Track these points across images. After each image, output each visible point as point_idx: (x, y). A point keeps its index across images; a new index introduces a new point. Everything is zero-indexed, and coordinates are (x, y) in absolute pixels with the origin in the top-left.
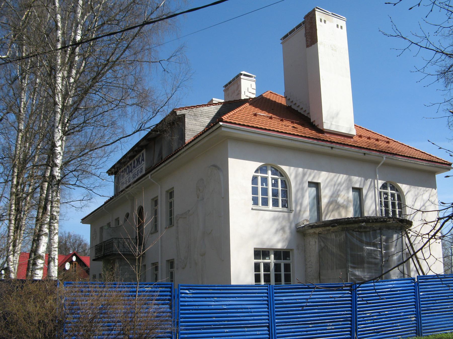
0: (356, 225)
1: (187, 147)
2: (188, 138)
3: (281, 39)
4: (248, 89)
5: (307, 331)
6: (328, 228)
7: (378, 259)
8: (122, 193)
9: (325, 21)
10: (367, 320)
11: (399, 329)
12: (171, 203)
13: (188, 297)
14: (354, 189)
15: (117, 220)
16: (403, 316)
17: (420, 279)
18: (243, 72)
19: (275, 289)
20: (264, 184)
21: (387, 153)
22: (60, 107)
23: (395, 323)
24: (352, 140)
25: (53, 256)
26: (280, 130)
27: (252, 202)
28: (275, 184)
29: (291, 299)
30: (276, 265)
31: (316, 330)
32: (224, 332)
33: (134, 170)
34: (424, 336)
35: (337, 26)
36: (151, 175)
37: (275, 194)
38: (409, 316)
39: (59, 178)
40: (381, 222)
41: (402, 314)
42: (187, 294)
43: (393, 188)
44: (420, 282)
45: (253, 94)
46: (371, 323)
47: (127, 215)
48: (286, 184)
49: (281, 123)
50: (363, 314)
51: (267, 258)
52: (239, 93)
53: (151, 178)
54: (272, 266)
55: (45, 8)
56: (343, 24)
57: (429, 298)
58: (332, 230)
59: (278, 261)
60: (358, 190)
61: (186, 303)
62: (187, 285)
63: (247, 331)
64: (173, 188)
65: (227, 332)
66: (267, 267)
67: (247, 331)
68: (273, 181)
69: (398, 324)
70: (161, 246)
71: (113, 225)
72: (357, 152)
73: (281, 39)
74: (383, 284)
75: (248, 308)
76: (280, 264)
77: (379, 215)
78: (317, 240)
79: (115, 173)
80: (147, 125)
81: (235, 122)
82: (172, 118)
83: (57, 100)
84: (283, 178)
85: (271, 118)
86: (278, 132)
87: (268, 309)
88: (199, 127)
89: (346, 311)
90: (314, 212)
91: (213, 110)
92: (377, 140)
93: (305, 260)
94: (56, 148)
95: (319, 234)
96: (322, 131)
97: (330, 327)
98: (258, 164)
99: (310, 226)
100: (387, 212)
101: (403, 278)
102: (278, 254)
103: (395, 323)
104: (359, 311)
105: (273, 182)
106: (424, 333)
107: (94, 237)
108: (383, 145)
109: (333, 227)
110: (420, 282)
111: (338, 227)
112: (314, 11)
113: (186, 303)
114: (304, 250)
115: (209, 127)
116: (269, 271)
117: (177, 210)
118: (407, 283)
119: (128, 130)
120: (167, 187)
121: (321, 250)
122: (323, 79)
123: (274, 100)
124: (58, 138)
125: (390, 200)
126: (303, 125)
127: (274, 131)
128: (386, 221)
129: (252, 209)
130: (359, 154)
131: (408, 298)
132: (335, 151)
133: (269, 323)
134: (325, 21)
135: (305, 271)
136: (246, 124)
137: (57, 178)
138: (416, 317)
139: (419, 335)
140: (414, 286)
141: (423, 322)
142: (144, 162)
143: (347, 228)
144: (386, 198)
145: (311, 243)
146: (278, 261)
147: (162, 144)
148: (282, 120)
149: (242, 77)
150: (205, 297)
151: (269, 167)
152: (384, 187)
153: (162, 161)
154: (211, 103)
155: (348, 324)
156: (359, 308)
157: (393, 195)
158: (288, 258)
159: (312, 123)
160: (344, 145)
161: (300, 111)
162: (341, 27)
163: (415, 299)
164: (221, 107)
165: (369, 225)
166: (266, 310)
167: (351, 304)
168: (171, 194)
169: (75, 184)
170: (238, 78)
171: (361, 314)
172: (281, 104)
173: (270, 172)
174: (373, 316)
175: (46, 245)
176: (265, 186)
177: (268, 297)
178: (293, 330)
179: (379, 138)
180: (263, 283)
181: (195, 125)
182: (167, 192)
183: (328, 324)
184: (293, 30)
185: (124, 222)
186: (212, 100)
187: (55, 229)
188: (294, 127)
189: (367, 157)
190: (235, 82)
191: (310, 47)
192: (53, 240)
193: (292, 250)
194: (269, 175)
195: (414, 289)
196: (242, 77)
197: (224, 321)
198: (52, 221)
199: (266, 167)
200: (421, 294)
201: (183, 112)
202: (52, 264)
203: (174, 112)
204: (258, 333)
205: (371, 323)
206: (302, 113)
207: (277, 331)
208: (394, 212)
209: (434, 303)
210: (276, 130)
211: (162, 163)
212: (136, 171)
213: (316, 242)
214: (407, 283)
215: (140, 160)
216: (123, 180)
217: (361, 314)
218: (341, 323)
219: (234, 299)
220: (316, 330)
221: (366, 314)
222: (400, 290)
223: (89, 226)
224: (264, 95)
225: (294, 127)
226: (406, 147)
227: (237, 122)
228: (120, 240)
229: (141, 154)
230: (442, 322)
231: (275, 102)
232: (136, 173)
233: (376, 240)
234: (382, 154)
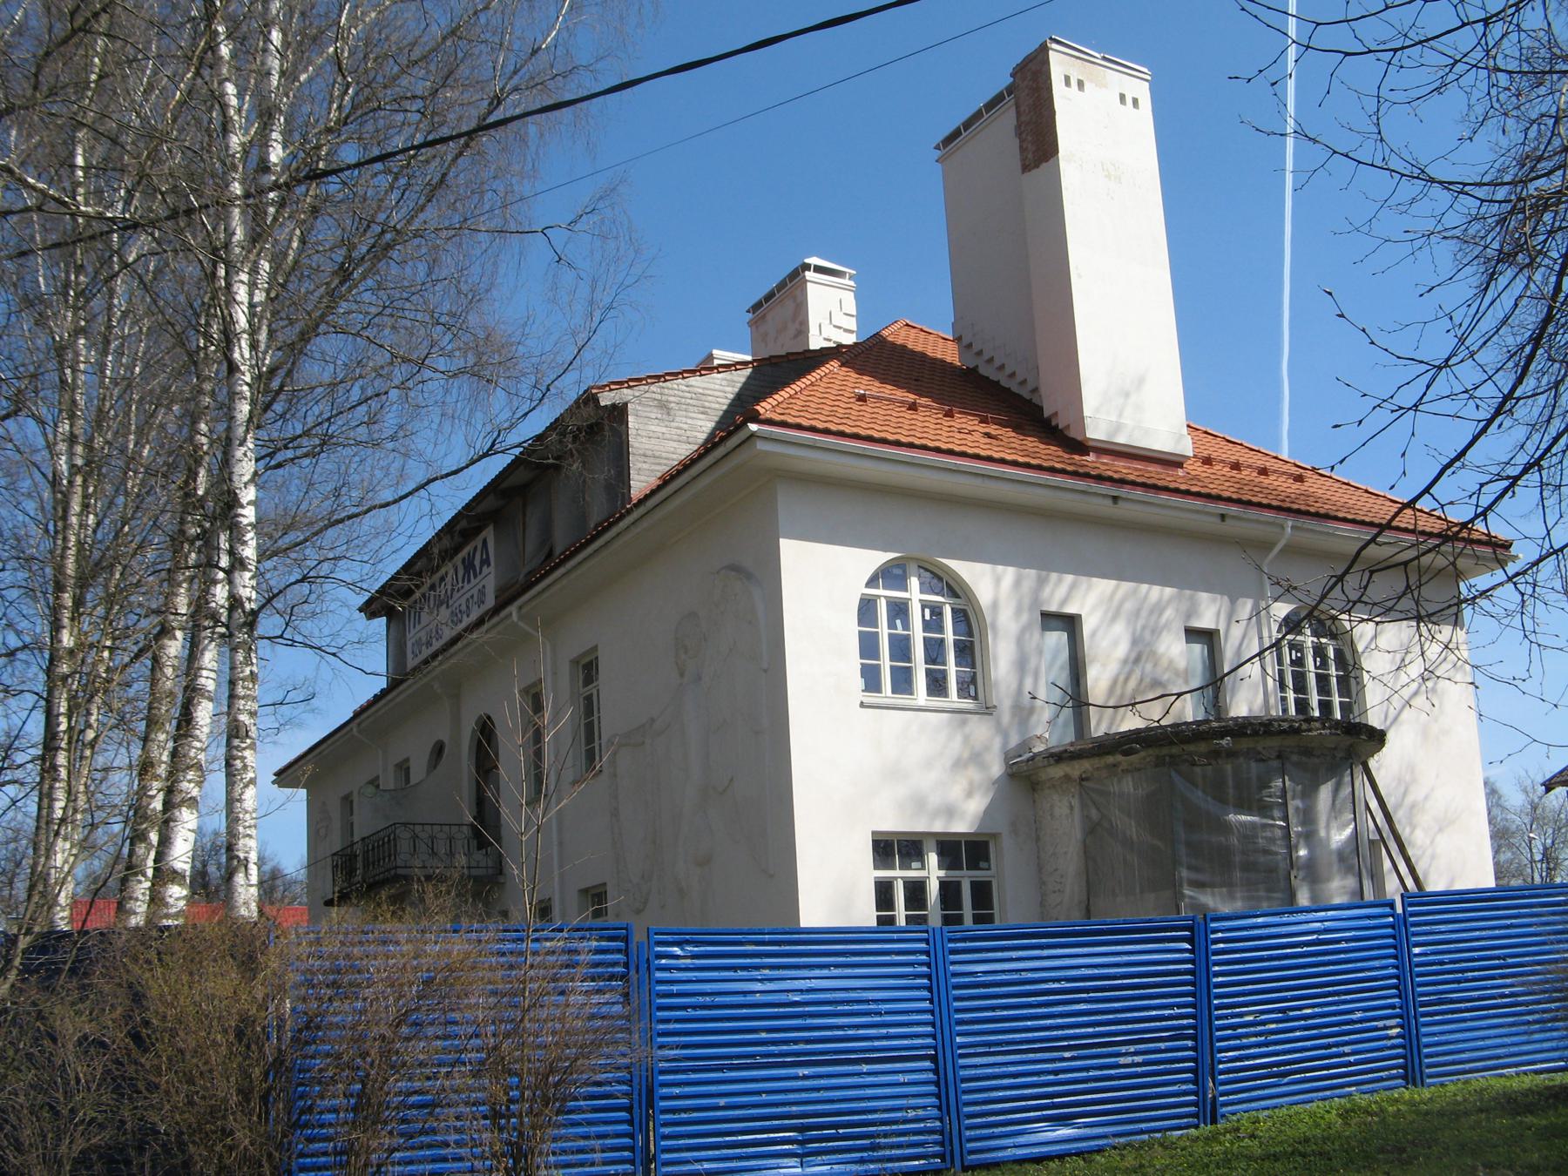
0: (1202, 747)
1: (642, 510)
2: (641, 480)
3: (938, 147)
4: (832, 314)
5: (1056, 1072)
6: (1110, 759)
7: (1277, 853)
8: (435, 663)
9: (1081, 84)
10: (1247, 1035)
11: (1350, 1064)
12: (589, 699)
13: (679, 969)
14: (1193, 634)
15: (403, 768)
16: (1360, 1021)
17: (1411, 905)
18: (814, 261)
19: (950, 940)
20: (898, 622)
21: (1299, 512)
22: (248, 379)
23: (1337, 1045)
24: (1180, 472)
25: (242, 855)
26: (944, 446)
27: (861, 683)
28: (934, 622)
29: (1003, 972)
30: (943, 885)
31: (1087, 1069)
32: (796, 1078)
33: (456, 595)
34: (1429, 1086)
35: (1122, 98)
36: (520, 608)
37: (934, 651)
38: (1380, 1024)
39: (253, 606)
40: (1284, 732)
41: (1359, 1015)
42: (677, 957)
44: (1412, 915)
45: (846, 331)
46: (1259, 1045)
47: (439, 749)
48: (968, 617)
49: (946, 422)
50: (1234, 1016)
51: (914, 865)
52: (803, 331)
53: (521, 618)
54: (933, 889)
56: (1142, 90)
57: (1442, 963)
58: (1124, 766)
60: (1206, 637)
61: (675, 988)
62: (674, 928)
63: (869, 1074)
64: (595, 648)
65: (805, 1077)
67: (869, 1074)
68: (927, 611)
69: (1347, 1049)
70: (561, 844)
71: (389, 781)
72: (1197, 512)
73: (938, 147)
74: (1292, 919)
75: (867, 1001)
76: (958, 884)
77: (1276, 712)
78: (1076, 802)
79: (390, 613)
80: (513, 438)
81: (798, 420)
82: (587, 411)
83: (237, 355)
85: (913, 407)
86: (938, 450)
87: (932, 1002)
88: (675, 444)
89: (1180, 1006)
90: (1065, 725)
91: (721, 390)
92: (1264, 472)
93: (1040, 868)
94: (240, 511)
95: (1082, 779)
96: (1080, 447)
97: (1129, 1060)
98: (879, 558)
99: (1052, 755)
100: (1302, 705)
101: (1357, 901)
102: (950, 848)
103: (1337, 1045)
104: (1219, 1007)
105: (927, 617)
106: (1431, 1076)
107: (322, 832)
108: (1283, 486)
109: (1126, 753)
110: (1412, 915)
111: (1143, 754)
112: (1044, 49)
113: (675, 988)
114: (1034, 833)
115: (710, 445)
116: (923, 906)
117: (610, 722)
118: (1369, 917)
119: (441, 459)
120: (574, 647)
121: (1092, 830)
122: (1079, 276)
123: (919, 349)
124: (246, 478)
125: (1312, 668)
126: (1018, 428)
127: (925, 448)
128: (1297, 731)
129: (862, 705)
130: (1201, 516)
131: (1376, 963)
132: (1125, 511)
133: (935, 1048)
134: (1081, 84)
135: (1042, 904)
136: (833, 427)
137: (247, 606)
138: (1402, 1026)
139: (1415, 1084)
140: (1392, 926)
141: (1425, 1040)
142: (492, 568)
143: (1171, 756)
144: (1299, 662)
145: (1057, 811)
147: (552, 503)
148: (949, 414)
149: (809, 275)
150: (734, 968)
151: (912, 567)
152: (1291, 625)
153: (550, 562)
154: (706, 367)
155: (1186, 1049)
156: (1216, 964)
157: (1319, 651)
158: (982, 864)
159: (1049, 420)
160: (1155, 488)
161: (1006, 385)
162: (1135, 102)
163: (1397, 967)
164: (749, 378)
165: (1245, 744)
166: (926, 1005)
167: (1193, 984)
168: (588, 669)
169: (281, 637)
170: (795, 278)
171: (1226, 1017)
172: (942, 361)
173: (914, 582)
174: (1264, 1023)
175: (192, 837)
176: (900, 631)
177: (928, 965)
178: (1012, 1069)
179: (1271, 464)
181: (665, 431)
182: (575, 662)
183: (1123, 1049)
184: (977, 115)
185: (428, 772)
186: (711, 357)
187: (245, 767)
188: (988, 435)
189: (1230, 527)
190: (786, 294)
191: (1034, 171)
192: (240, 800)
193: (995, 836)
194: (914, 593)
195: (1394, 937)
196: (809, 275)
197: (796, 1041)
198: (236, 742)
200: (1416, 950)
201: (626, 394)
202: (240, 878)
203: (589, 398)
204: (901, 1078)
205: (1259, 1045)
206: (1015, 389)
207: (962, 1073)
208: (1326, 706)
209: (1458, 981)
210: (931, 444)
211: (553, 569)
212: (463, 601)
213: (1072, 808)
214: (1369, 917)
215: (477, 563)
216: (412, 635)
217: (1226, 1017)
218: (1162, 1045)
219: (825, 972)
220: (1087, 1069)
221: (1241, 1015)
222: (1347, 940)
223: (302, 793)
224: (885, 333)
225: (988, 435)
226: (1359, 493)
227: (805, 423)
228: (418, 829)
229: (478, 542)
230: (1489, 1042)
231: (923, 355)
232: (464, 608)
233: (1265, 792)
234: (1281, 516)
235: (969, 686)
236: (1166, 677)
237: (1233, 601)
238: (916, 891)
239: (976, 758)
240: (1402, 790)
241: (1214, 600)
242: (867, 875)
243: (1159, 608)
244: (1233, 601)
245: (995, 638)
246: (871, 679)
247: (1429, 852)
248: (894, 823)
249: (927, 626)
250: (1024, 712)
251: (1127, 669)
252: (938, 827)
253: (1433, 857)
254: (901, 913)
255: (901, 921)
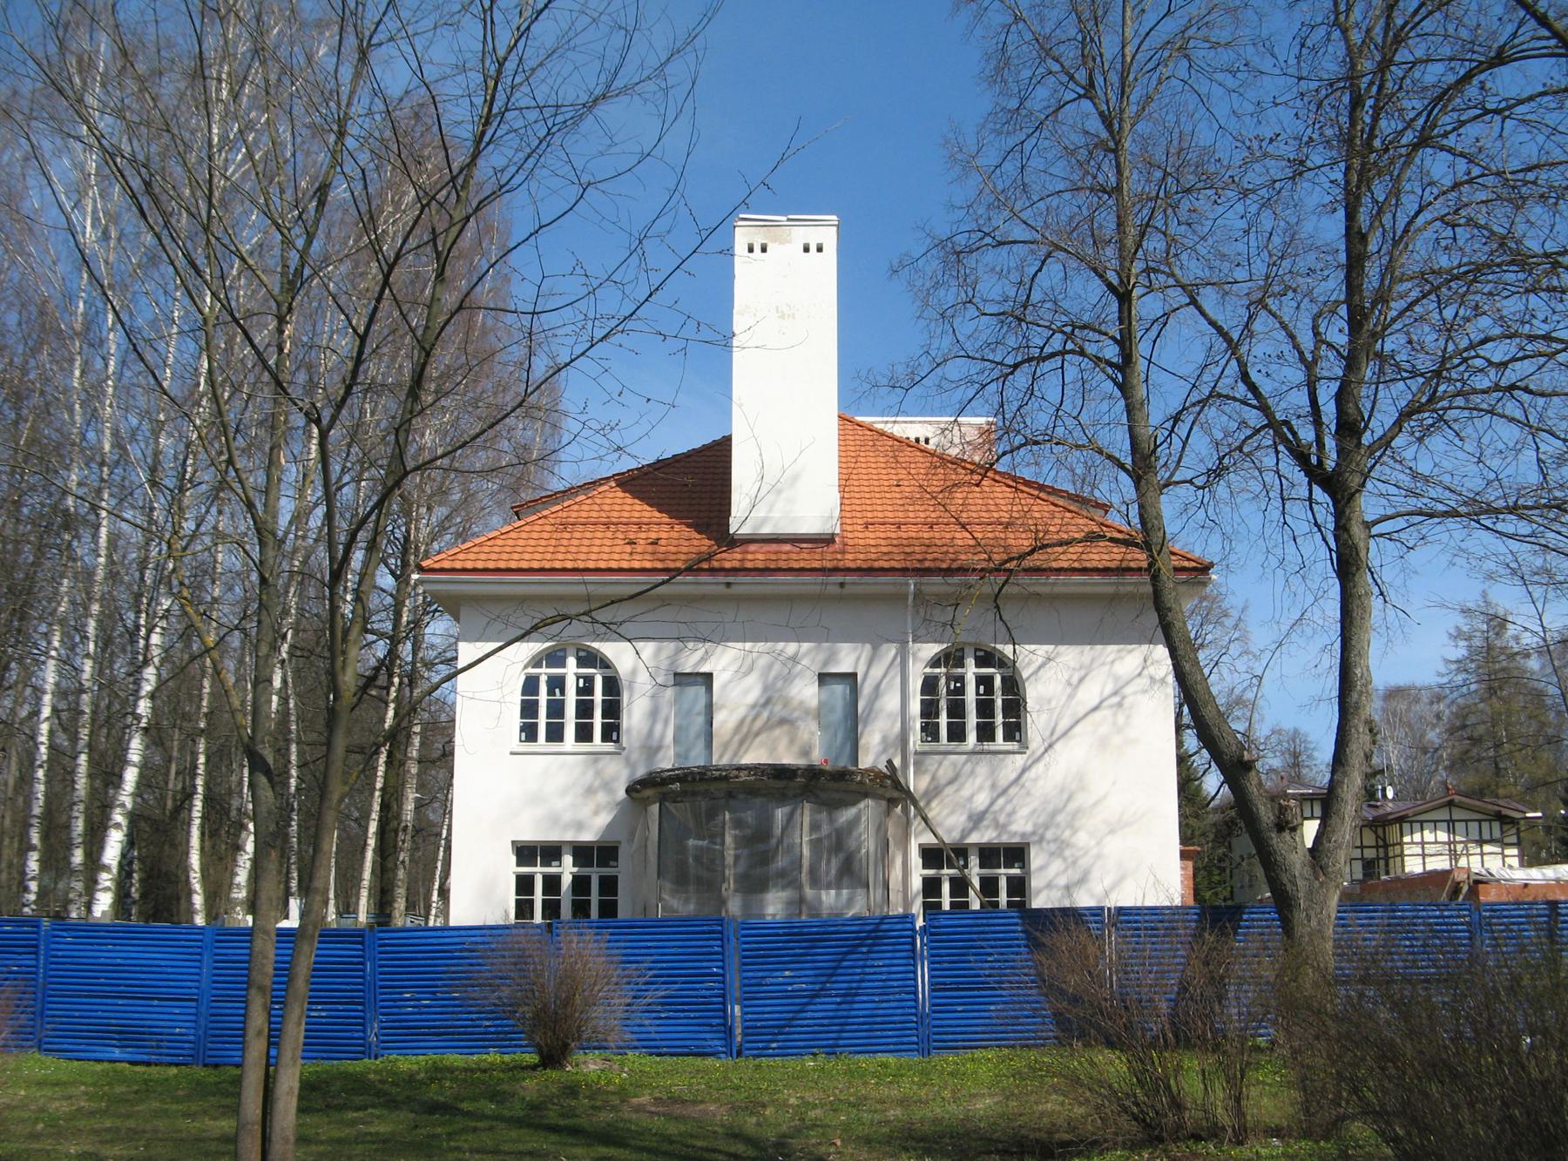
30: (576, 878)
43: (985, 659)
54: (567, 880)
55: (1460, 243)
59: (586, 871)
66: (552, 883)
76: (949, 740)
84: (609, 673)
102: (583, 853)
134: (764, 250)
146: (586, 871)
173: (571, 661)
176: (558, 696)
180: (538, 918)
194: (571, 669)
199: (564, 650)
235: (611, 732)
236: (796, 714)
237: (875, 648)
238: (552, 883)
239: (607, 786)
240: (1065, 796)
241: (855, 649)
242: (509, 868)
243: (794, 659)
244: (875, 648)
245: (631, 696)
246: (529, 733)
247: (1094, 851)
248: (531, 833)
249: (579, 691)
250: (652, 750)
251: (753, 713)
252: (569, 836)
253: (1099, 857)
254: (1003, 898)
255: (946, 906)
